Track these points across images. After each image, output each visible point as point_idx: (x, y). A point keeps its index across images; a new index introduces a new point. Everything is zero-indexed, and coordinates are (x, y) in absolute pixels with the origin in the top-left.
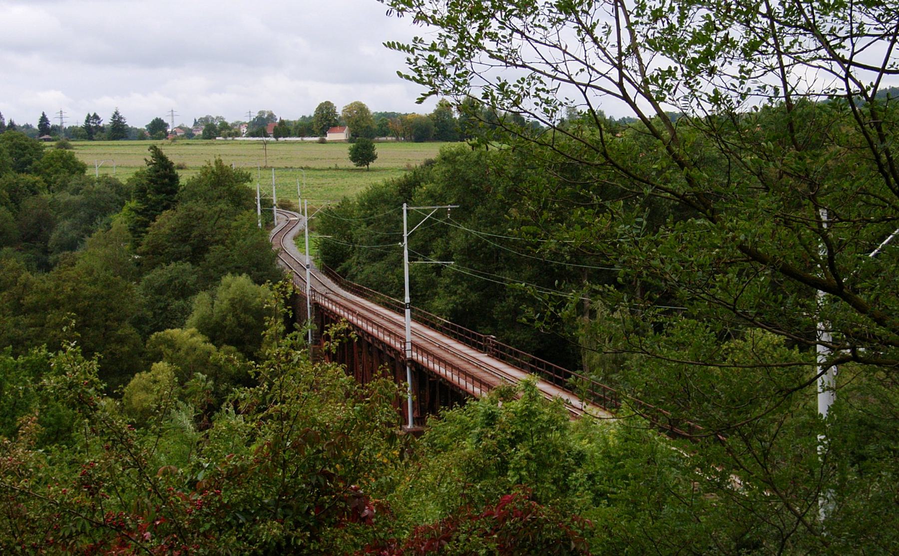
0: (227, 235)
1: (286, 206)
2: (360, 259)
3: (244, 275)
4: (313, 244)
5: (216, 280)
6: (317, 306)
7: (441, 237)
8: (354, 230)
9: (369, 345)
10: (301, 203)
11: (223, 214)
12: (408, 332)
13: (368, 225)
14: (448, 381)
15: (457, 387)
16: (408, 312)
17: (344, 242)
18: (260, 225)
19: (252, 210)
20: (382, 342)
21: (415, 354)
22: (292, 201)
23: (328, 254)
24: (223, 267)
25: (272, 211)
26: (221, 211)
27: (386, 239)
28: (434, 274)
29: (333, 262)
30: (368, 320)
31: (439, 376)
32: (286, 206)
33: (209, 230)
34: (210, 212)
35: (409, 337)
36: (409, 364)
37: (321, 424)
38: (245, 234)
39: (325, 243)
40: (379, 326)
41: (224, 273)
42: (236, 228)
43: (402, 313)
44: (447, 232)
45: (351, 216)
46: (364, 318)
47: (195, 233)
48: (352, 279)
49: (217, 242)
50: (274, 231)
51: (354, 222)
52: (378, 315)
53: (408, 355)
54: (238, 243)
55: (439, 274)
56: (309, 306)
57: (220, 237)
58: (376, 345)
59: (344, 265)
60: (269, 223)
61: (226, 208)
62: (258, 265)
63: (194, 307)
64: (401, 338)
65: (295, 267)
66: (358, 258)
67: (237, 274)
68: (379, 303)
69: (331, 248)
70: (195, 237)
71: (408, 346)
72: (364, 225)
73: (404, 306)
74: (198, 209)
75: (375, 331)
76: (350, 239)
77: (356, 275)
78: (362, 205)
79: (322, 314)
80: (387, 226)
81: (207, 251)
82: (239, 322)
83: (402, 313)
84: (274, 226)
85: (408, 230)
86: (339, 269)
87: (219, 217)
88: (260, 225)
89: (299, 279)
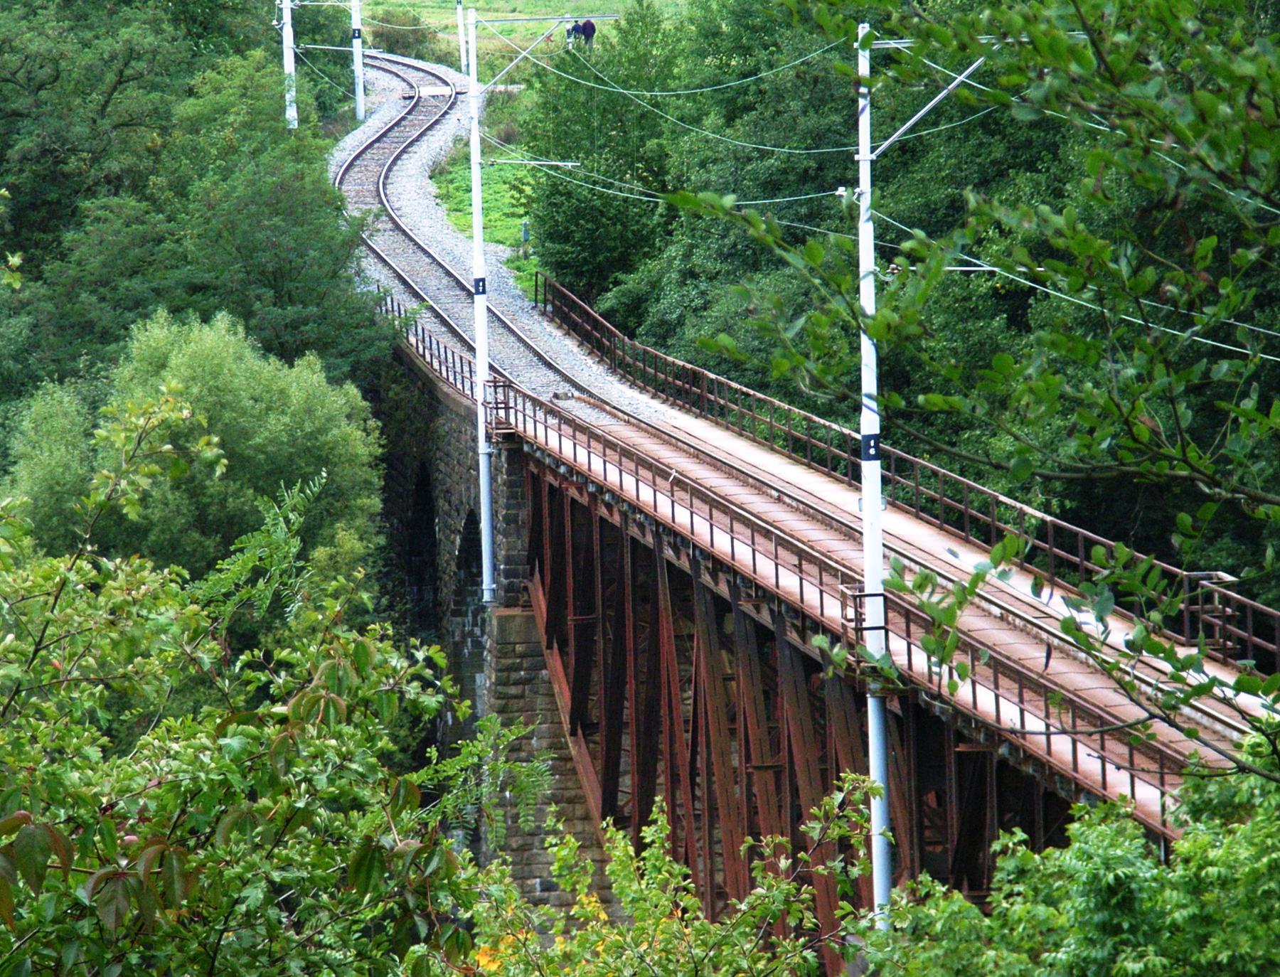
0: (154, 153)
1: (402, 40)
2: (697, 259)
3: (222, 319)
4: (508, 197)
5: (106, 337)
6: (514, 446)
7: (1031, 167)
8: (676, 135)
9: (722, 607)
10: (465, 31)
11: (141, 66)
12: (855, 547)
13: (730, 119)
14: (1031, 758)
15: (1065, 779)
16: (871, 470)
17: (630, 189)
18: (291, 113)
19: (258, 54)
20: (767, 596)
21: (898, 645)
22: (431, 20)
23: (566, 238)
24: (135, 285)
25: (345, 60)
26: (132, 54)
27: (804, 177)
28: (999, 321)
29: (589, 269)
30: (716, 504)
31: (995, 733)
32: (402, 40)
33: (81, 130)
34: (88, 57)
35: (874, 575)
36: (874, 686)
37: (79, 800)
38: (229, 150)
39: (555, 192)
40: (760, 530)
41: (139, 308)
42: (193, 126)
43: (853, 477)
44: (1053, 149)
45: (664, 76)
46: (698, 493)
47: (24, 144)
48: (662, 341)
49: (115, 183)
50: (352, 143)
51: (676, 104)
52: (760, 486)
53: (873, 644)
54: (197, 187)
55: (1019, 323)
56: (483, 447)
57: (128, 160)
58: (748, 608)
59: (632, 282)
60: (332, 112)
61: (150, 40)
62: (279, 281)
63: (17, 446)
64: (846, 579)
65: (431, 283)
66: (687, 256)
67: (193, 316)
68: (768, 441)
69: (578, 214)
70: (24, 158)
71: (874, 612)
72: (713, 119)
73: (858, 450)
74: (37, 45)
75: (743, 554)
76: (655, 171)
77: (681, 321)
78: (711, 34)
79: (536, 480)
80: (810, 122)
81: (74, 217)
82: (202, 510)
83: (853, 477)
84: (351, 122)
85: (875, 140)
86: (609, 300)
87: (121, 81)
88: (291, 113)
89: (446, 339)
